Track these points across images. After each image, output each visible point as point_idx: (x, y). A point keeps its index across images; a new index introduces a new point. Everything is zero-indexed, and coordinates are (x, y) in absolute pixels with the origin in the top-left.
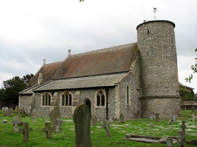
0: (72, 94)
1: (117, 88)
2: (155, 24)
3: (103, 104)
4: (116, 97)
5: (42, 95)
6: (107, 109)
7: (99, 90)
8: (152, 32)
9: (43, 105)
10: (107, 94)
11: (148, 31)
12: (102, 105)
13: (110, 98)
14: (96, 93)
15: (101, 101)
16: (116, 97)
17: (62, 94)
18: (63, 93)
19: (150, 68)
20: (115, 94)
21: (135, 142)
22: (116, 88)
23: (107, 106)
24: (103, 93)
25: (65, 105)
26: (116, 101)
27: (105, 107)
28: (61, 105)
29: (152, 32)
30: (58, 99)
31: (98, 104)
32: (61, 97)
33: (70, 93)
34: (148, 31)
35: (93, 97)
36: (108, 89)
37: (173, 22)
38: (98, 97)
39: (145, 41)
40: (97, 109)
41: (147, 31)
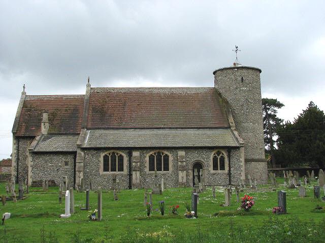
0: (170, 155)
1: (242, 150)
2: (250, 71)
3: (223, 168)
4: (241, 160)
5: (103, 155)
6: (229, 174)
7: (217, 150)
8: (247, 81)
9: (106, 169)
10: (229, 156)
11: (242, 78)
12: (123, 171)
13: (233, 160)
14: (212, 155)
15: (218, 164)
16: (241, 160)
17: (104, 154)
18: (151, 153)
19: (245, 125)
20: (240, 157)
21: (198, 203)
22: (241, 148)
23: (230, 170)
24: (223, 154)
25: (117, 170)
26: (241, 164)
27: (226, 171)
28: (147, 170)
29: (247, 81)
30: (142, 163)
31: (215, 168)
32: (147, 159)
33: (166, 152)
34: (242, 78)
35: (208, 159)
36: (229, 149)
37: (260, 68)
38: (215, 160)
39: (238, 91)
40: (214, 174)
41: (240, 79)
